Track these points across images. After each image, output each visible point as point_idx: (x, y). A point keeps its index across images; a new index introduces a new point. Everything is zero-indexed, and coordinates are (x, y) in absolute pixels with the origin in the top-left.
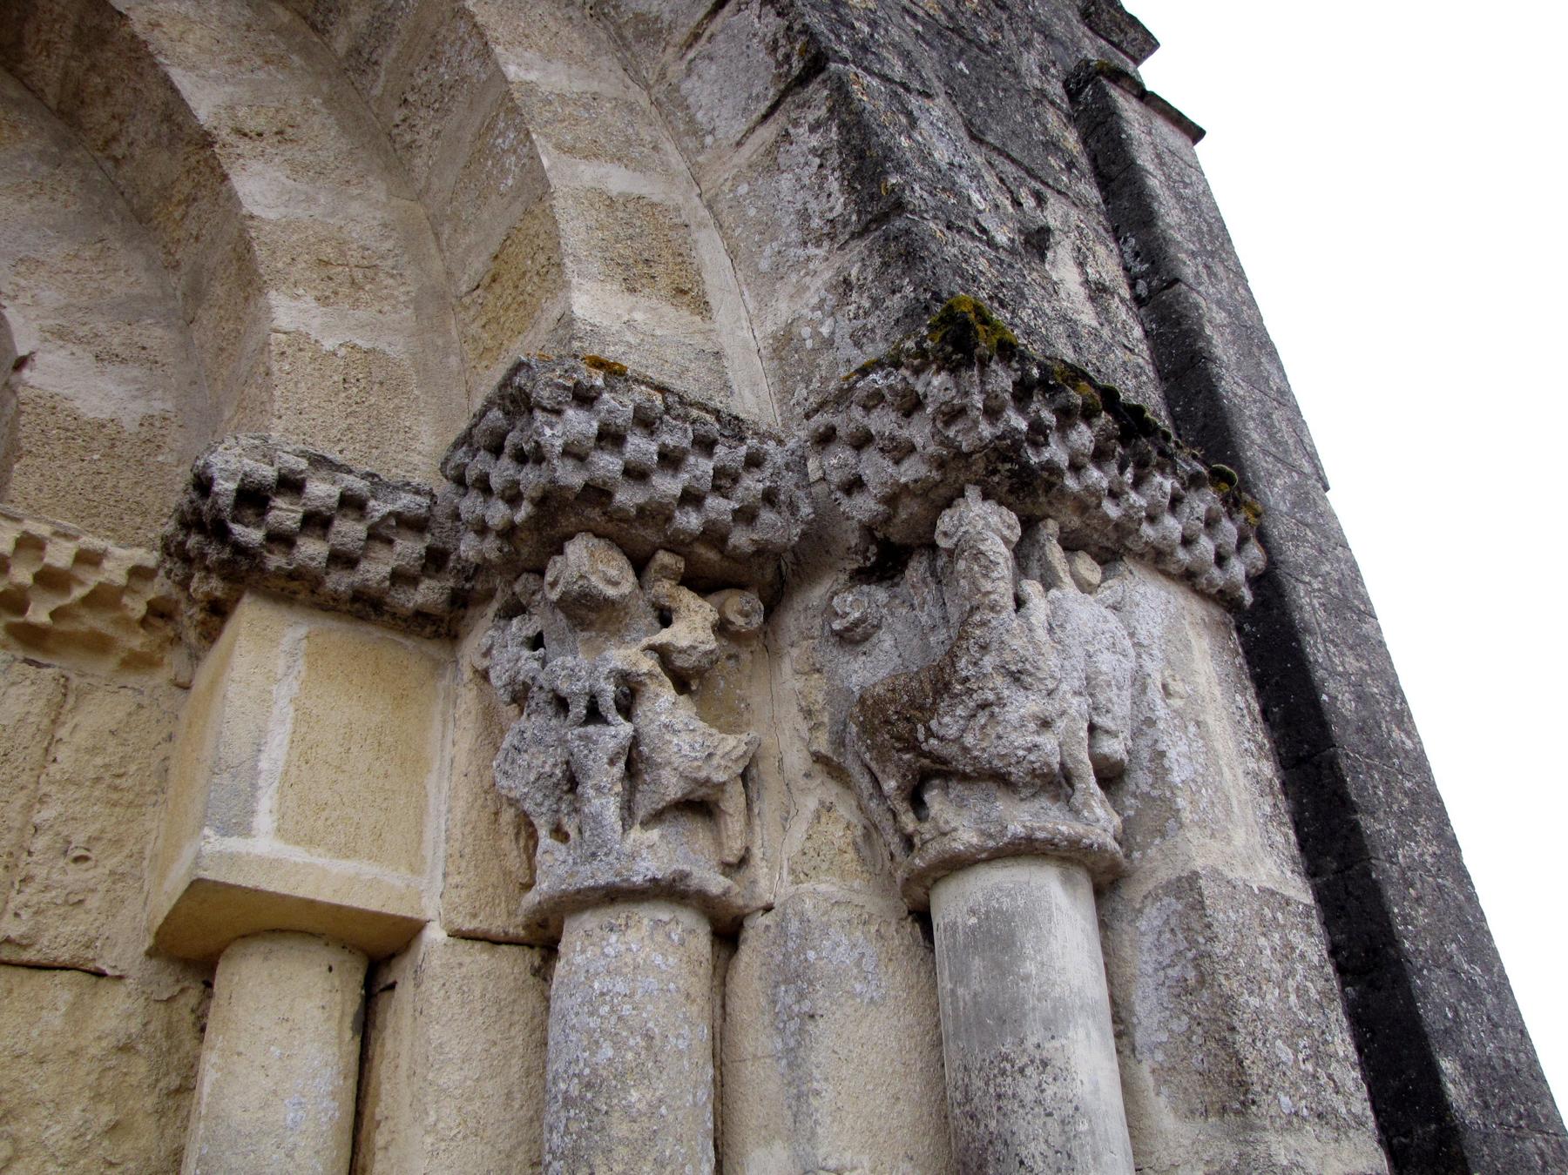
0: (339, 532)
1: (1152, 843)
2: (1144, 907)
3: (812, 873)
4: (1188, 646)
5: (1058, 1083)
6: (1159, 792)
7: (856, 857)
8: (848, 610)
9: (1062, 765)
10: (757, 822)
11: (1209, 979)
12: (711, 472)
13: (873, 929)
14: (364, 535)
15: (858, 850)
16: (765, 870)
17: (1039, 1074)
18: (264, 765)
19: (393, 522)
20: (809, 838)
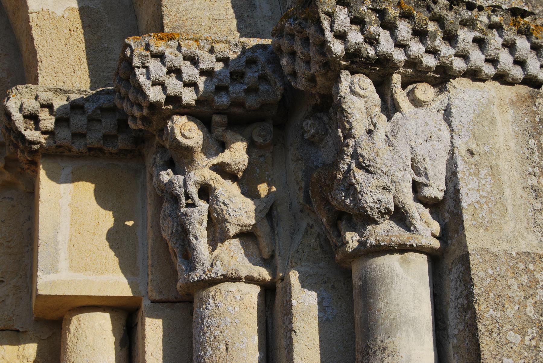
0: (74, 124)
4: (493, 122)
5: (390, 358)
8: (309, 129)
9: (396, 206)
10: (277, 238)
12: (228, 75)
13: (330, 285)
14: (86, 122)
16: (281, 261)
17: (382, 354)
18: (60, 238)
19: (99, 112)
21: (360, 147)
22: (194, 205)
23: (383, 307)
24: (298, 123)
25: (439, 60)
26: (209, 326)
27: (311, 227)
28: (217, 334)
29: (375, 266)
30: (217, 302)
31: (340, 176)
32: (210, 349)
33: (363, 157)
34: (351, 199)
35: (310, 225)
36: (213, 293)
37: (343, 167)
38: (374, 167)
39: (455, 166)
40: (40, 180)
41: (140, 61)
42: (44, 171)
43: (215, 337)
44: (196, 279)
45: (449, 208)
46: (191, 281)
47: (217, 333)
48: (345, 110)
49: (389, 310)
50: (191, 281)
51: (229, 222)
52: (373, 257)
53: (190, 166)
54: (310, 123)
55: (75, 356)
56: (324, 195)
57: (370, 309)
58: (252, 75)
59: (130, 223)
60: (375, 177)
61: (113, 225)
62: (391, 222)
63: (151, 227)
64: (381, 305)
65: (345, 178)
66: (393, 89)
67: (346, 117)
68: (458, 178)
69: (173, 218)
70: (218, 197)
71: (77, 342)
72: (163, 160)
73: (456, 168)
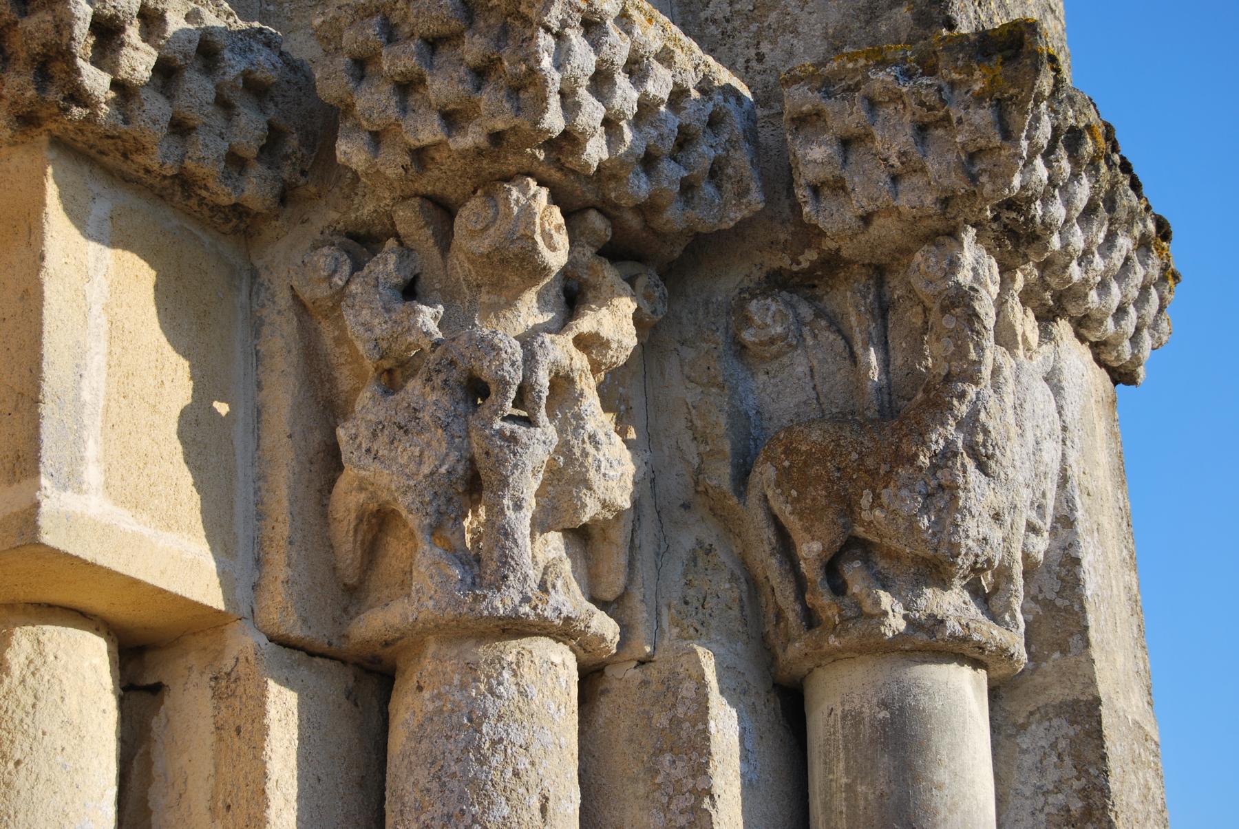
1: (1048, 656)
2: (1029, 724)
3: (702, 630)
6: (1067, 602)
7: (739, 615)
11: (1097, 813)
15: (742, 608)
20: (689, 584)
21: (985, 408)
22: (530, 422)
23: (947, 781)
24: (720, 298)
25: (1086, 273)
26: (501, 740)
27: (708, 552)
28: (523, 767)
29: (930, 684)
30: (523, 683)
31: (924, 460)
32: (504, 802)
33: (986, 432)
34: (933, 518)
35: (706, 546)
36: (511, 658)
37: (937, 442)
38: (997, 462)
39: (1068, 506)
40: (47, 210)
41: (560, 17)
42: (55, 186)
43: (516, 774)
44: (501, 612)
45: (1041, 591)
46: (486, 613)
47: (523, 763)
48: (979, 318)
49: (960, 791)
50: (486, 613)
51: (590, 489)
52: (925, 662)
53: (492, 315)
54: (773, 308)
55: (26, 746)
56: (845, 489)
57: (916, 779)
58: (704, 153)
59: (222, 408)
60: (992, 485)
61: (190, 401)
62: (965, 592)
63: (290, 436)
64: (942, 775)
65: (934, 467)
66: (1007, 301)
67: (978, 333)
68: (1076, 533)
69: (453, 437)
70: (582, 419)
71: (34, 706)
72: (402, 274)
73: (1071, 510)
